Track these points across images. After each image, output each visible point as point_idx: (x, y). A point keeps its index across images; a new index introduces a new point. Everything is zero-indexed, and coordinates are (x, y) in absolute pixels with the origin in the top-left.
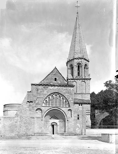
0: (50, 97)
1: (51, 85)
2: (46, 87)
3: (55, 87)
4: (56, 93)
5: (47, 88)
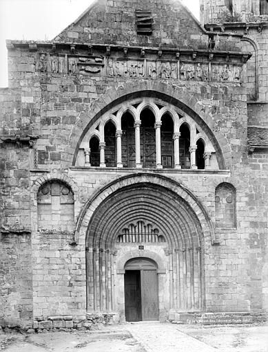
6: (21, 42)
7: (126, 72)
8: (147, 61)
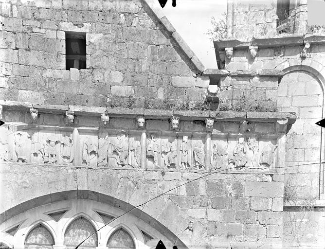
0: (50, 223)
3: (68, 132)
6: (264, 126)
7: (36, 154)
8: (80, 131)
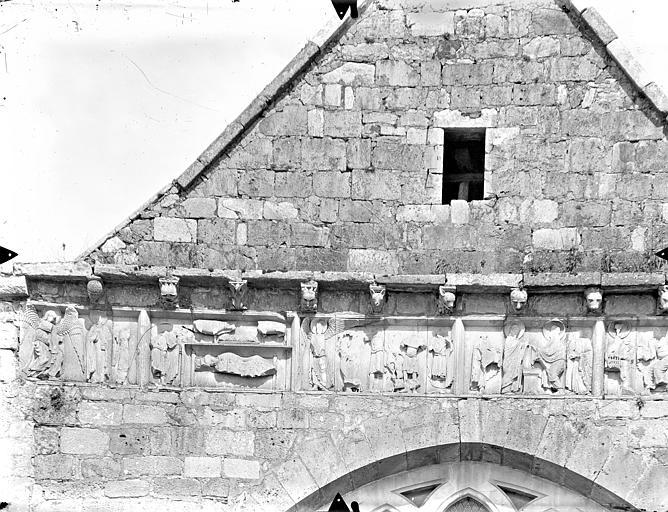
1: (357, 290)
2: (247, 334)
4: (473, 453)
5: (256, 365)
